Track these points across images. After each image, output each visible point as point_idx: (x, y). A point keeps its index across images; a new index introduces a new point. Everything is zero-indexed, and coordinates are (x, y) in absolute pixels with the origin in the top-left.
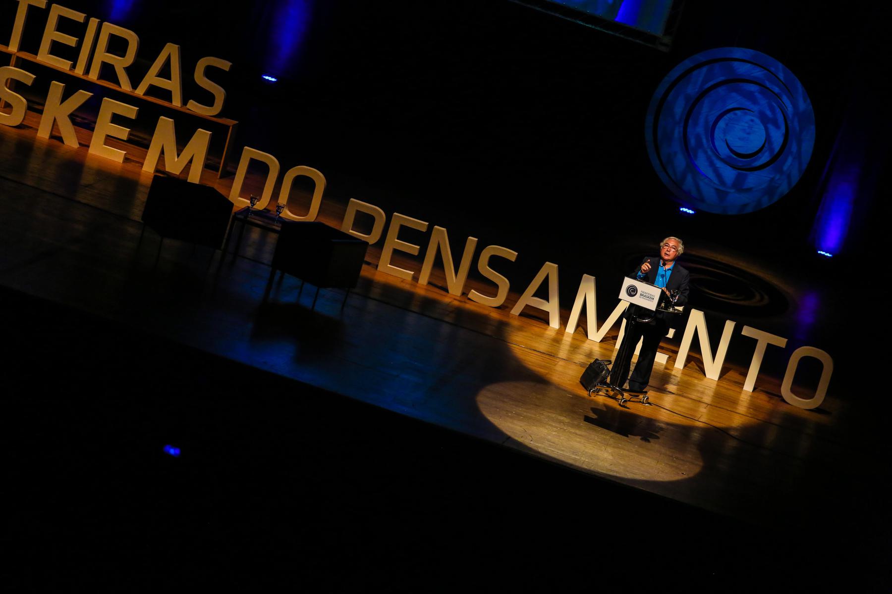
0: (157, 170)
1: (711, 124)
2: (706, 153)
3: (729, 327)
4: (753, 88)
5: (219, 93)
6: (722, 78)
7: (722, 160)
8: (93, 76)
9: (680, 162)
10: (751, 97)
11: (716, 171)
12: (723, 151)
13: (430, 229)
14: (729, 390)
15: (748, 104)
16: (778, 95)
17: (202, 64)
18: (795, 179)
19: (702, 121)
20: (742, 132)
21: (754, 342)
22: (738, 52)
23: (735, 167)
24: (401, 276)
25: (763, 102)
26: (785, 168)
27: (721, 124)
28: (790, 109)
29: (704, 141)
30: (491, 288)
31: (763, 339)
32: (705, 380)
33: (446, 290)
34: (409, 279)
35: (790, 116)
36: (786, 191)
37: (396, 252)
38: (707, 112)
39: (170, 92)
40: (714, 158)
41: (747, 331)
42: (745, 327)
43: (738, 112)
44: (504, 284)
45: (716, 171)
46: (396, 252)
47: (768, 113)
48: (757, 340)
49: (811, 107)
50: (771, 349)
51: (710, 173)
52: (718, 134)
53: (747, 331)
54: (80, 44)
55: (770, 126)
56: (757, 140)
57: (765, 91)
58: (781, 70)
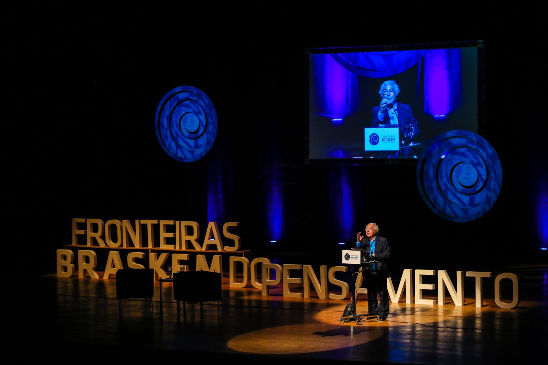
1: (449, 175)
2: (451, 191)
3: (459, 274)
4: (188, 102)
5: (235, 238)
6: (175, 103)
7: (460, 193)
8: (184, 248)
9: (440, 200)
10: (188, 106)
11: (459, 199)
12: (459, 188)
14: (469, 309)
15: (463, 159)
16: (197, 101)
17: (226, 226)
18: (498, 191)
19: (175, 125)
20: (189, 126)
21: (474, 278)
22: (177, 89)
23: (467, 195)
24: (297, 296)
25: (470, 155)
26: (492, 187)
27: (454, 174)
28: (484, 155)
29: (448, 185)
31: (478, 276)
32: (456, 308)
33: (318, 298)
34: (299, 297)
35: (486, 158)
36: (496, 199)
37: (290, 284)
38: (175, 119)
39: (216, 245)
40: (457, 193)
41: (469, 274)
42: (467, 272)
43: (460, 165)
44: (344, 285)
45: (459, 199)
46: (290, 284)
47: (475, 160)
48: (475, 278)
49: (495, 151)
50: (483, 280)
51: (457, 202)
52: (454, 179)
53: (469, 274)
54: (175, 235)
55: (199, 115)
56: (474, 177)
57: (470, 150)
58: (194, 90)
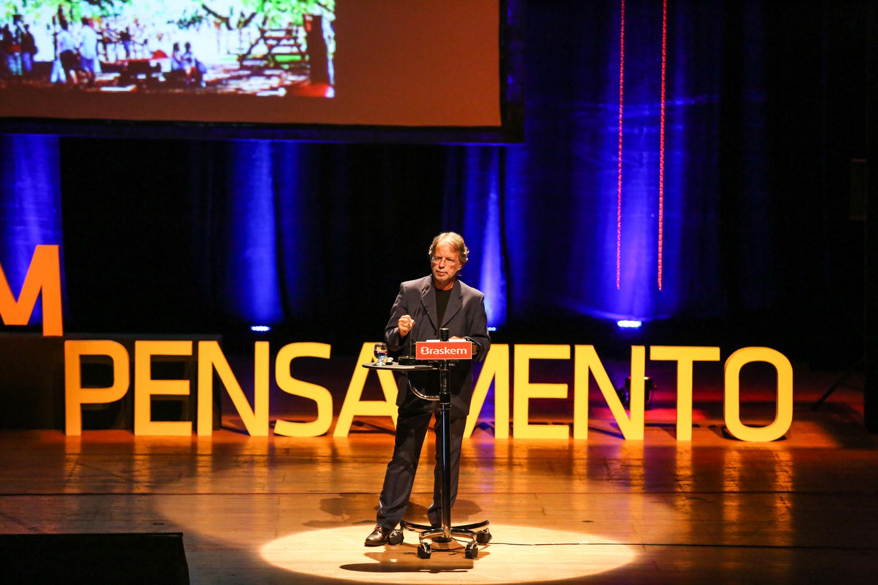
0: (265, 466)
13: (195, 349)
30: (305, 409)
31: (685, 357)
44: (321, 396)
50: (699, 367)
53: (660, 353)
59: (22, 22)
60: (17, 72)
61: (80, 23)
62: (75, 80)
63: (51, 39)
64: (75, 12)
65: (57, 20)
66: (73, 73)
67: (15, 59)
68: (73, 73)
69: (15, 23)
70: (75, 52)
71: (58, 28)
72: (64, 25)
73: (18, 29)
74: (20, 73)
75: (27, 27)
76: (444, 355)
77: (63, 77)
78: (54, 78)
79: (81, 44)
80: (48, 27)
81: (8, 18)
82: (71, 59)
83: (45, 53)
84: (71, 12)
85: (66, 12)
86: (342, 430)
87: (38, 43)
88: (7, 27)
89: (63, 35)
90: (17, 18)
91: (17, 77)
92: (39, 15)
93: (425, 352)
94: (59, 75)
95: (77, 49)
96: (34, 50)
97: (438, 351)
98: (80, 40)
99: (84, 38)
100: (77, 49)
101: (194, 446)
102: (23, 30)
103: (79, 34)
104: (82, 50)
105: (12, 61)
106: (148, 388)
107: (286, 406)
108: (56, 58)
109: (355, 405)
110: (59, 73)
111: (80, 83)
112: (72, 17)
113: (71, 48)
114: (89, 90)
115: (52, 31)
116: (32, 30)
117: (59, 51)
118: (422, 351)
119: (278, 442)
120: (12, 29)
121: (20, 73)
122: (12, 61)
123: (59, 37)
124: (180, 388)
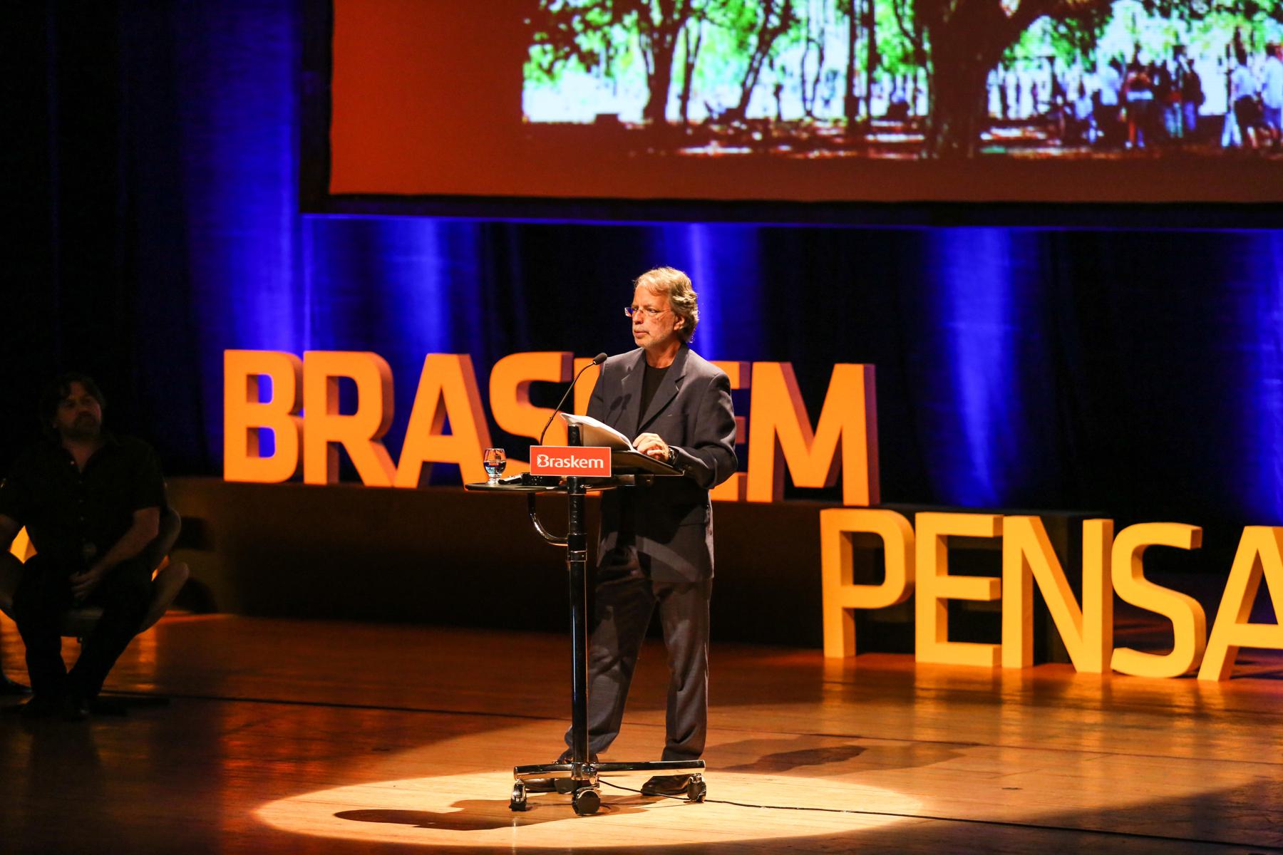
13: (998, 525)
44: (1179, 608)
59: (1185, 55)
60: (1176, 133)
61: (1263, 53)
62: (1255, 143)
63: (1223, 79)
64: (1257, 36)
65: (1232, 51)
66: (1251, 131)
67: (1174, 113)
68: (1251, 131)
69: (1175, 58)
70: (1255, 98)
71: (1234, 61)
72: (1242, 58)
73: (1180, 66)
74: (1180, 135)
75: (1191, 63)
76: (563, 470)
77: (1238, 138)
78: (1225, 141)
79: (1264, 86)
80: (1220, 62)
81: (1166, 51)
82: (1251, 109)
83: (1215, 102)
84: (1252, 37)
85: (1245, 37)
86: (1211, 671)
87: (1206, 87)
88: (1165, 64)
89: (1240, 73)
90: (1179, 50)
91: (1176, 140)
92: (1208, 44)
93: (543, 463)
94: (1232, 135)
95: (1259, 94)
96: (1199, 98)
97: (561, 463)
98: (1263, 80)
99: (1269, 76)
100: (1259, 94)
101: (997, 682)
102: (1186, 67)
103: (1261, 70)
104: (1264, 95)
105: (1169, 116)
106: (937, 587)
107: (1137, 630)
108: (1229, 108)
109: (1233, 630)
110: (1232, 133)
111: (1261, 147)
112: (1253, 44)
113: (1250, 92)
114: (1274, 158)
115: (1224, 69)
116: (1198, 68)
117: (1233, 98)
118: (539, 461)
119: (1118, 683)
120: (1172, 67)
121: (1180, 135)
122: (1169, 116)
123: (1234, 77)
124: (975, 589)
